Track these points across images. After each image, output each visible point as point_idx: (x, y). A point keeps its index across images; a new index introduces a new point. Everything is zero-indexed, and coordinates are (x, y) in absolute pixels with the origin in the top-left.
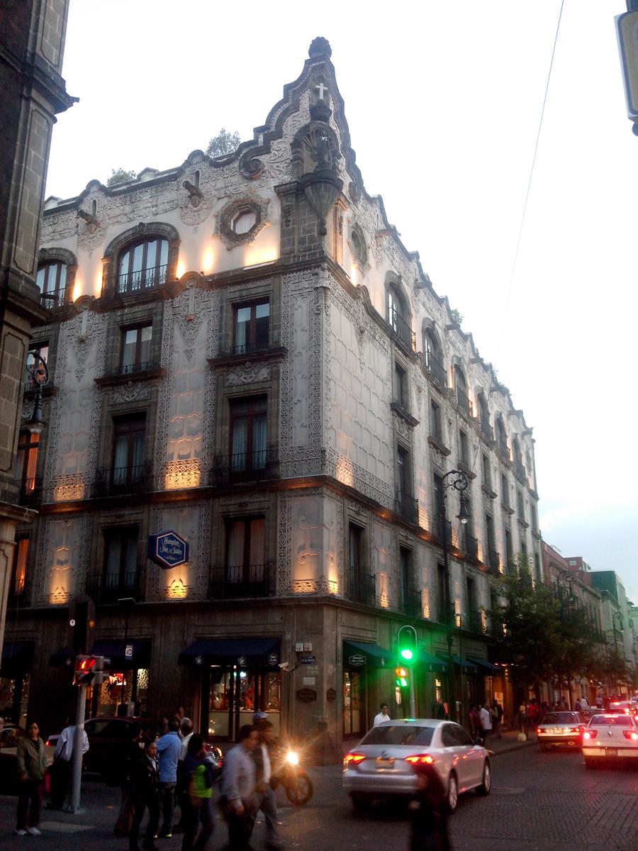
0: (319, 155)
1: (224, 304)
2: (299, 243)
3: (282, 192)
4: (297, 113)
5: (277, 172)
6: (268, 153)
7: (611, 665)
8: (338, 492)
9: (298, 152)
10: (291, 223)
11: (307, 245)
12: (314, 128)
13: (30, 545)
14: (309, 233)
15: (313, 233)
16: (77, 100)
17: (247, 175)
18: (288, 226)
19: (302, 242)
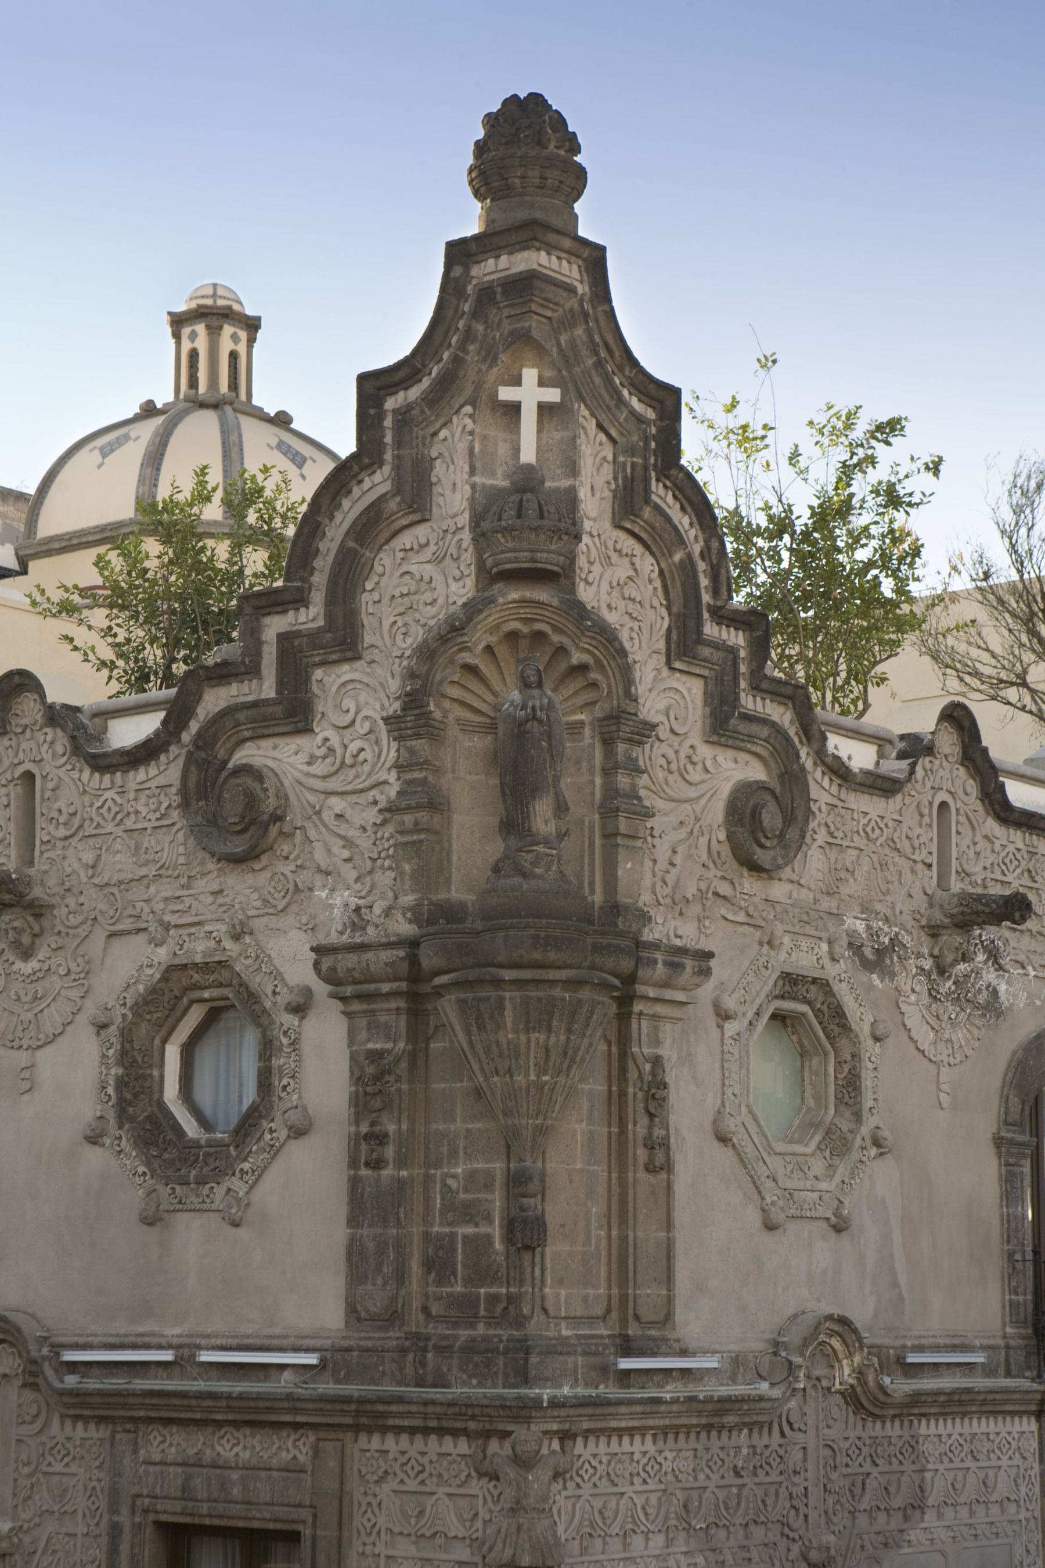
0: (521, 765)
1: (124, 1518)
2: (429, 1265)
3: (342, 968)
4: (422, 532)
5: (336, 845)
6: (297, 732)
7: (820, 506)
8: (668, 484)
9: (424, 764)
10: (390, 1152)
11: (459, 1288)
12: (494, 629)
13: (517, 451)
14: (471, 1220)
15: (484, 1229)
16: (169, 313)
17: (238, 845)
18: (376, 1164)
19: (439, 1264)
